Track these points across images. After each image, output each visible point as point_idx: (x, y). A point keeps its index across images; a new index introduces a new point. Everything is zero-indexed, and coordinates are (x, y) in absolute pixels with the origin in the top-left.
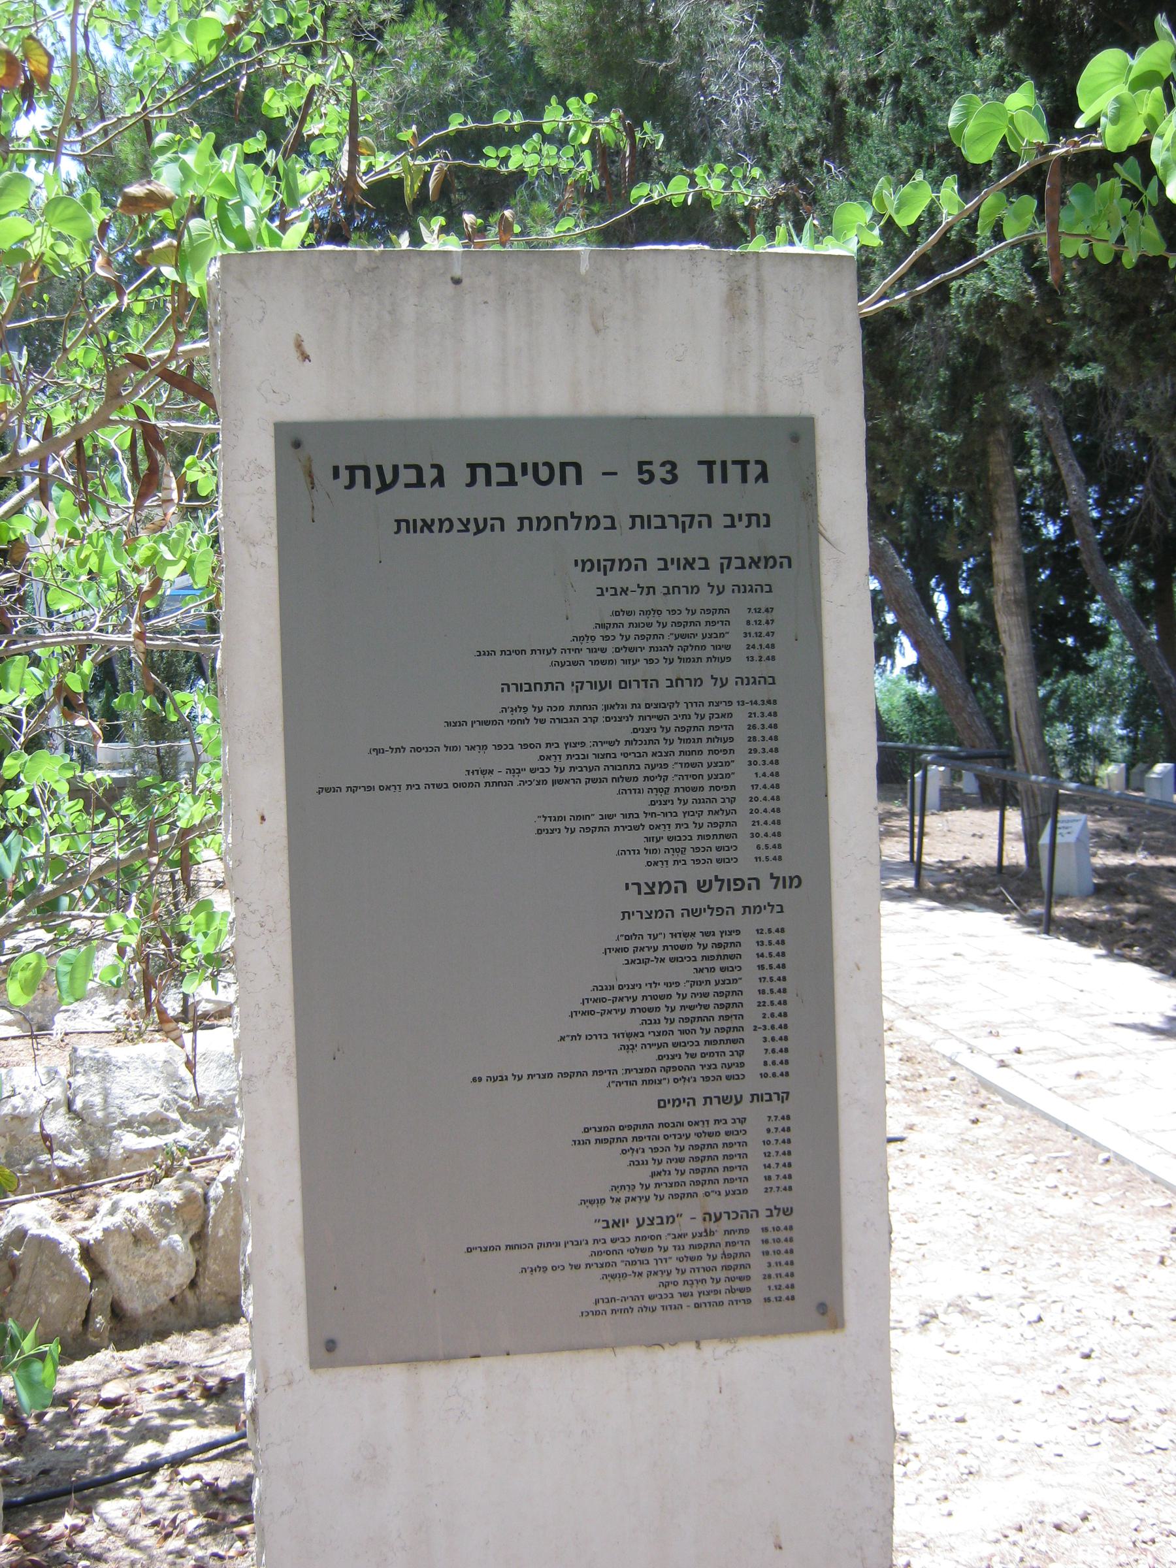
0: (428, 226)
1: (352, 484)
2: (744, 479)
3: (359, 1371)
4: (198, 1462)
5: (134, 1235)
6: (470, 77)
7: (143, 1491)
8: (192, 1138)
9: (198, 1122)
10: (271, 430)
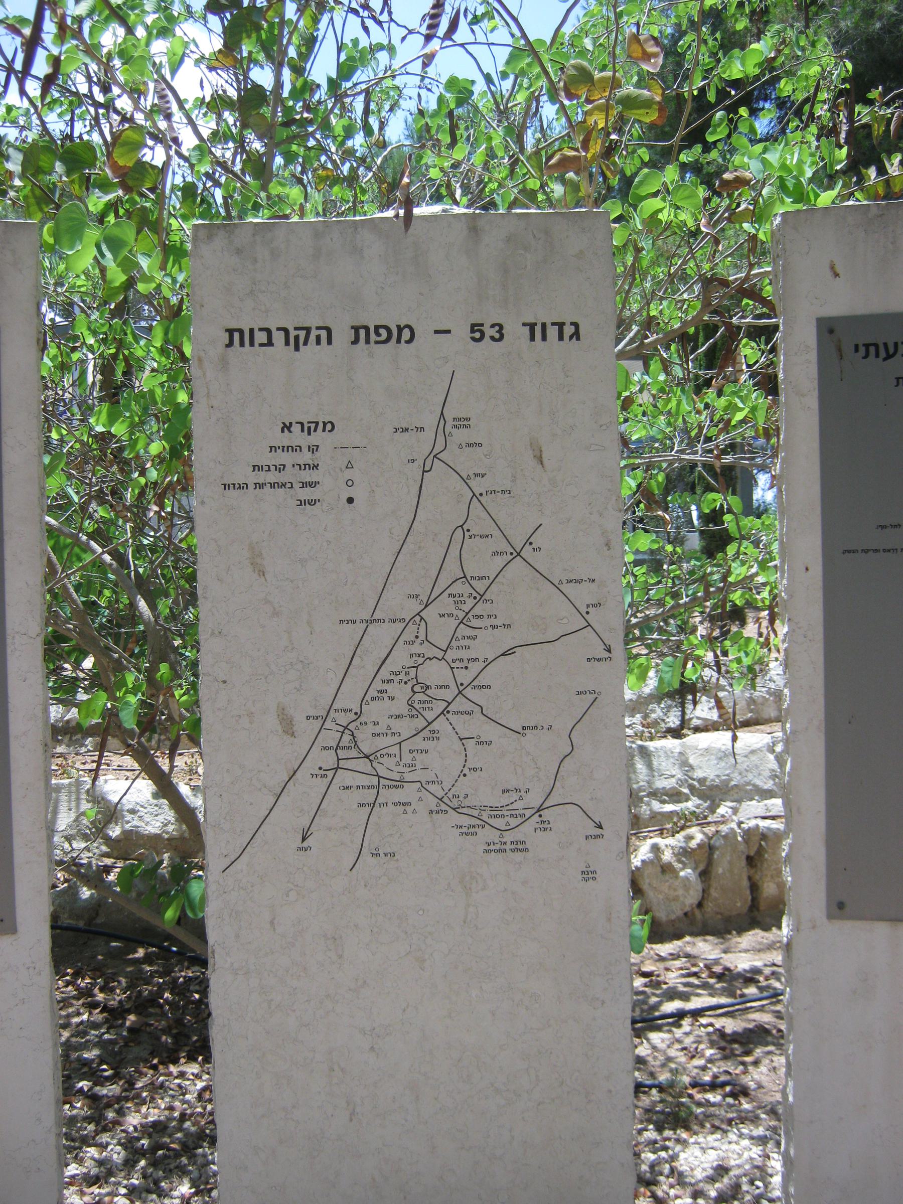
0: (889, 160)
1: (866, 356)
2: (561, 338)
3: (858, 924)
4: (710, 1016)
5: (662, 867)
6: (894, 15)
7: (674, 1029)
8: (698, 807)
9: (702, 796)
10: (814, 323)
